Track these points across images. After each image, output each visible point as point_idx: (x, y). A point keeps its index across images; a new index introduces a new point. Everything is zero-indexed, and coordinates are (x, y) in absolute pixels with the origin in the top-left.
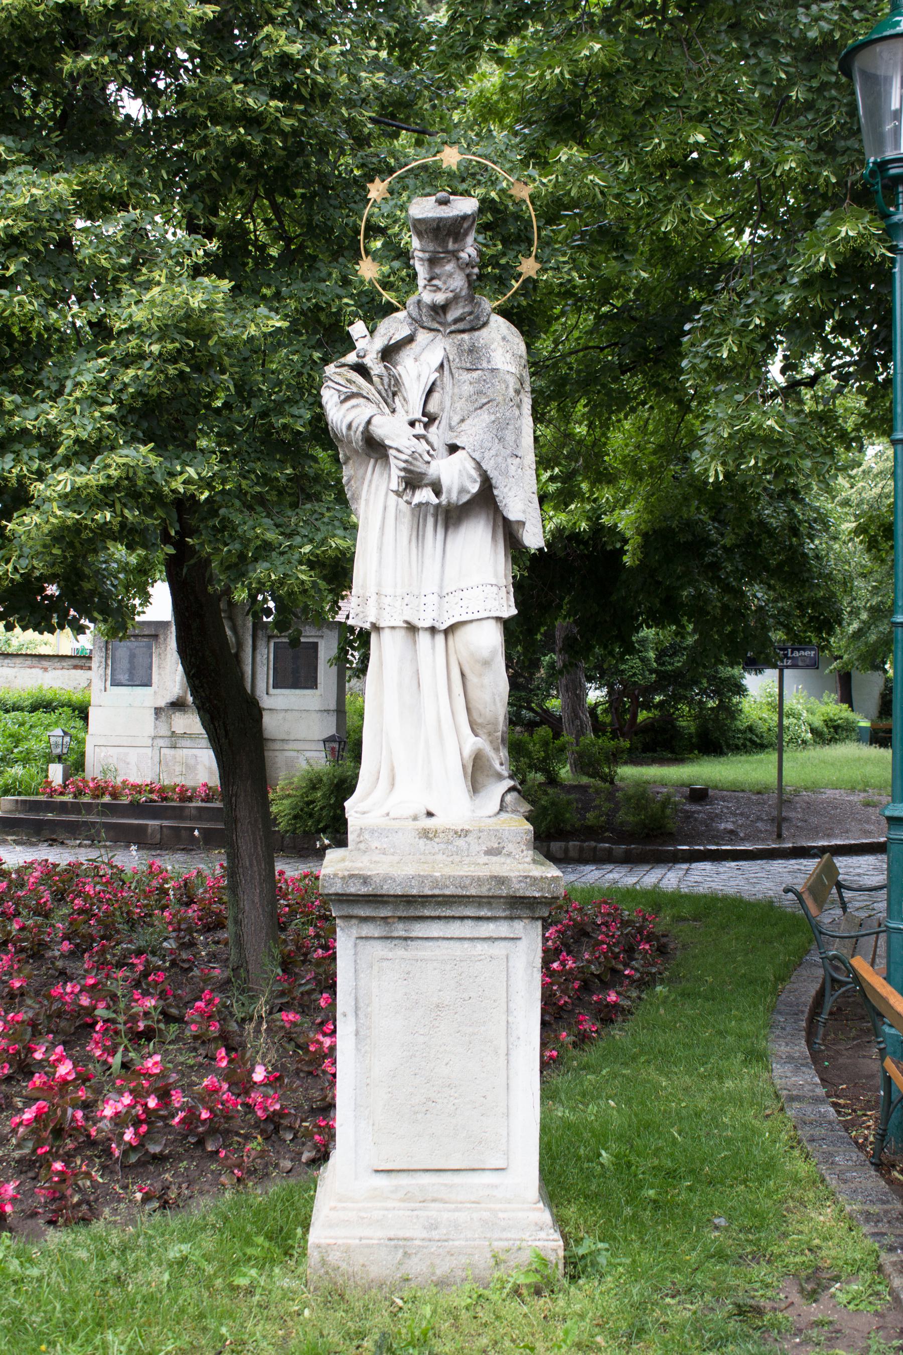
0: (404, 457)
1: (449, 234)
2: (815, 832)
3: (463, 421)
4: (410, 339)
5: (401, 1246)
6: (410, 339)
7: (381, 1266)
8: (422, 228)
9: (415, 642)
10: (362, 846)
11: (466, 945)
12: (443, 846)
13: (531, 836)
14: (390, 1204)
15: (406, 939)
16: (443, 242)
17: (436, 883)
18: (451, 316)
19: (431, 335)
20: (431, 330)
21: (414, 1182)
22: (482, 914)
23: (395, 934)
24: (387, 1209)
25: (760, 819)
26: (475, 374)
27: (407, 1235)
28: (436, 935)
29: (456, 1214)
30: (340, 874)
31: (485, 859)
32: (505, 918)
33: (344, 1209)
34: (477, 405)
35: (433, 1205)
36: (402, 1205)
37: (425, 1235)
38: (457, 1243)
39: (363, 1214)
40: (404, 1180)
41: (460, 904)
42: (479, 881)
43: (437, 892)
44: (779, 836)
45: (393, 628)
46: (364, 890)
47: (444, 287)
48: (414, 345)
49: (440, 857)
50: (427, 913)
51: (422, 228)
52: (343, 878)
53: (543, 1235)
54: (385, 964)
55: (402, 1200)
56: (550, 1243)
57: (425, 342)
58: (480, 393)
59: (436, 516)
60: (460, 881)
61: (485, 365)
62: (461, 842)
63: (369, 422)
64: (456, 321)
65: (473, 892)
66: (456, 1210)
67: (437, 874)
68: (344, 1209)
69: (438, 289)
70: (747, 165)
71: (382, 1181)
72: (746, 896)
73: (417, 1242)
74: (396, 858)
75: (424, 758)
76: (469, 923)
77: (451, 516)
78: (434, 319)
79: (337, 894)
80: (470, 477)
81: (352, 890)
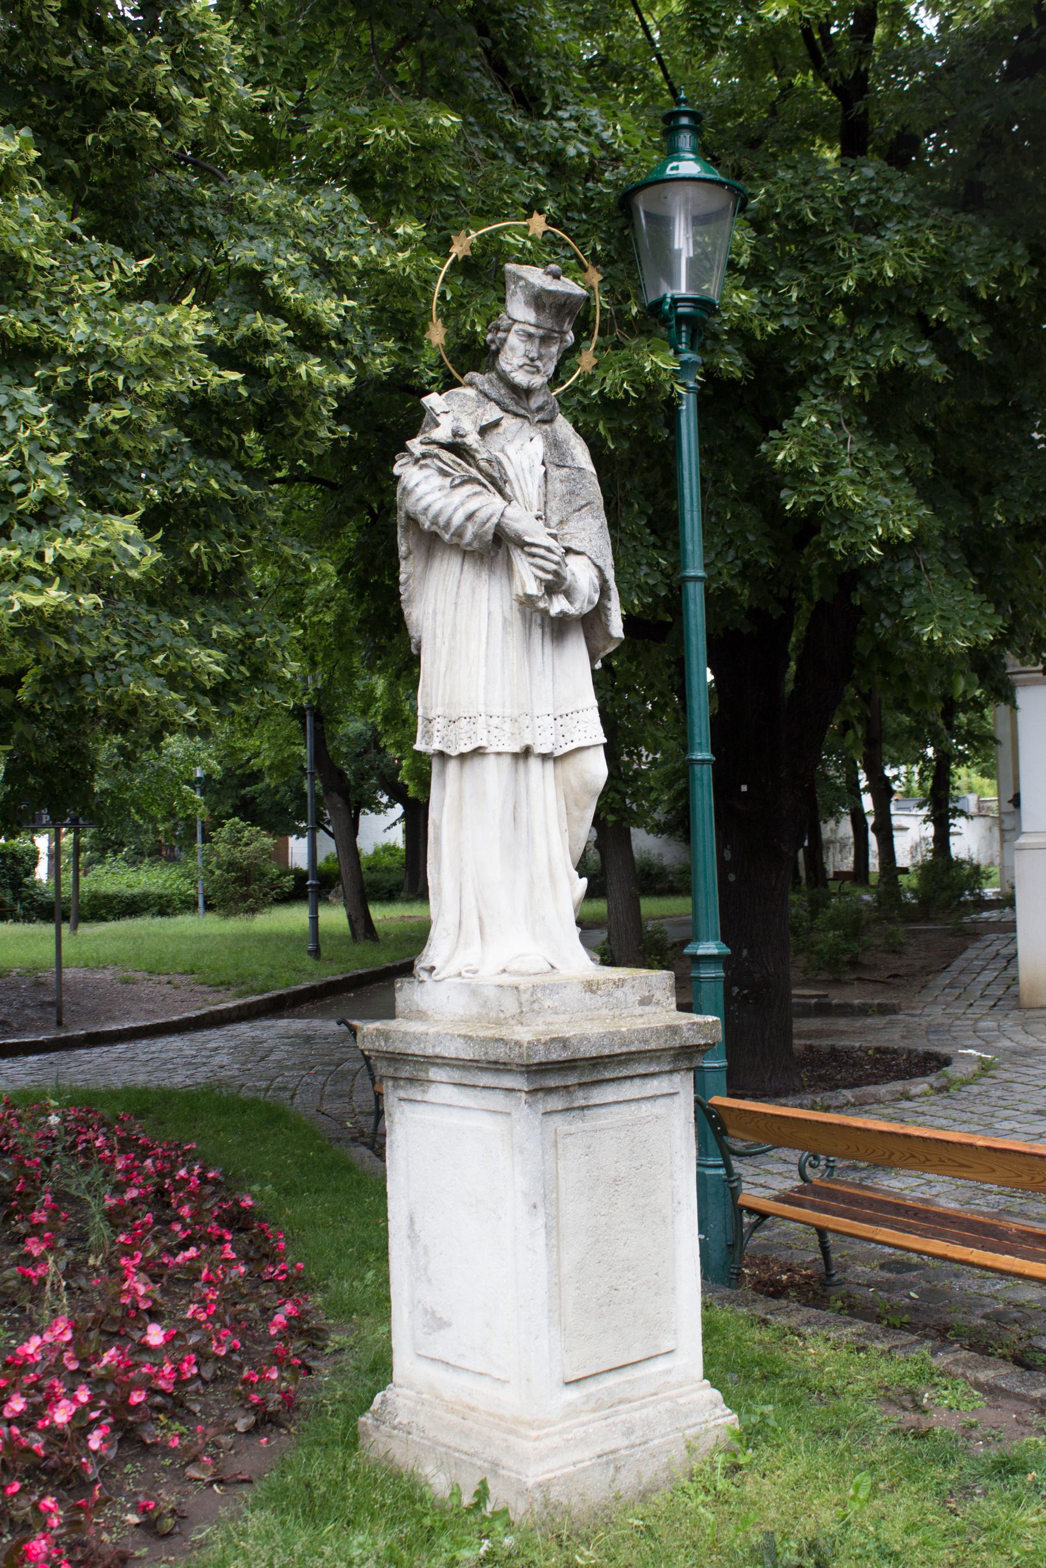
2: (94, 1015)
4: (496, 424)
5: (609, 1459)
6: (496, 424)
7: (597, 1489)
8: (547, 301)
9: (517, 770)
10: (536, 1006)
11: (634, 1107)
12: (605, 999)
13: (672, 982)
14: (585, 1418)
15: (582, 1108)
17: (624, 1040)
18: (535, 402)
19: (519, 420)
20: (516, 415)
21: (601, 1386)
22: (651, 1070)
23: (576, 1104)
24: (584, 1424)
25: (25, 1006)
27: (613, 1447)
28: (611, 1100)
29: (645, 1411)
30: (543, 1039)
31: (639, 1010)
32: (666, 1072)
33: (547, 1435)
34: (575, 506)
35: (621, 1407)
36: (597, 1415)
37: (626, 1443)
38: (656, 1442)
39: (566, 1436)
40: (591, 1388)
41: (638, 1061)
42: (656, 1032)
43: (625, 1049)
44: (59, 1023)
45: (499, 754)
46: (565, 1055)
48: (500, 430)
49: (604, 1012)
50: (608, 1075)
51: (547, 301)
52: (545, 1043)
53: (718, 1412)
54: (569, 1140)
55: (594, 1410)
56: (727, 1419)
58: (571, 493)
60: (641, 1035)
61: (570, 463)
62: (619, 993)
64: (540, 409)
65: (653, 1046)
66: (643, 1407)
67: (624, 1029)
68: (547, 1435)
69: (538, 371)
71: (573, 1394)
72: (152, 1086)
73: (623, 1452)
74: (567, 1017)
75: (505, 903)
76: (637, 1082)
77: (558, 628)
78: (517, 404)
79: (541, 1064)
81: (554, 1057)
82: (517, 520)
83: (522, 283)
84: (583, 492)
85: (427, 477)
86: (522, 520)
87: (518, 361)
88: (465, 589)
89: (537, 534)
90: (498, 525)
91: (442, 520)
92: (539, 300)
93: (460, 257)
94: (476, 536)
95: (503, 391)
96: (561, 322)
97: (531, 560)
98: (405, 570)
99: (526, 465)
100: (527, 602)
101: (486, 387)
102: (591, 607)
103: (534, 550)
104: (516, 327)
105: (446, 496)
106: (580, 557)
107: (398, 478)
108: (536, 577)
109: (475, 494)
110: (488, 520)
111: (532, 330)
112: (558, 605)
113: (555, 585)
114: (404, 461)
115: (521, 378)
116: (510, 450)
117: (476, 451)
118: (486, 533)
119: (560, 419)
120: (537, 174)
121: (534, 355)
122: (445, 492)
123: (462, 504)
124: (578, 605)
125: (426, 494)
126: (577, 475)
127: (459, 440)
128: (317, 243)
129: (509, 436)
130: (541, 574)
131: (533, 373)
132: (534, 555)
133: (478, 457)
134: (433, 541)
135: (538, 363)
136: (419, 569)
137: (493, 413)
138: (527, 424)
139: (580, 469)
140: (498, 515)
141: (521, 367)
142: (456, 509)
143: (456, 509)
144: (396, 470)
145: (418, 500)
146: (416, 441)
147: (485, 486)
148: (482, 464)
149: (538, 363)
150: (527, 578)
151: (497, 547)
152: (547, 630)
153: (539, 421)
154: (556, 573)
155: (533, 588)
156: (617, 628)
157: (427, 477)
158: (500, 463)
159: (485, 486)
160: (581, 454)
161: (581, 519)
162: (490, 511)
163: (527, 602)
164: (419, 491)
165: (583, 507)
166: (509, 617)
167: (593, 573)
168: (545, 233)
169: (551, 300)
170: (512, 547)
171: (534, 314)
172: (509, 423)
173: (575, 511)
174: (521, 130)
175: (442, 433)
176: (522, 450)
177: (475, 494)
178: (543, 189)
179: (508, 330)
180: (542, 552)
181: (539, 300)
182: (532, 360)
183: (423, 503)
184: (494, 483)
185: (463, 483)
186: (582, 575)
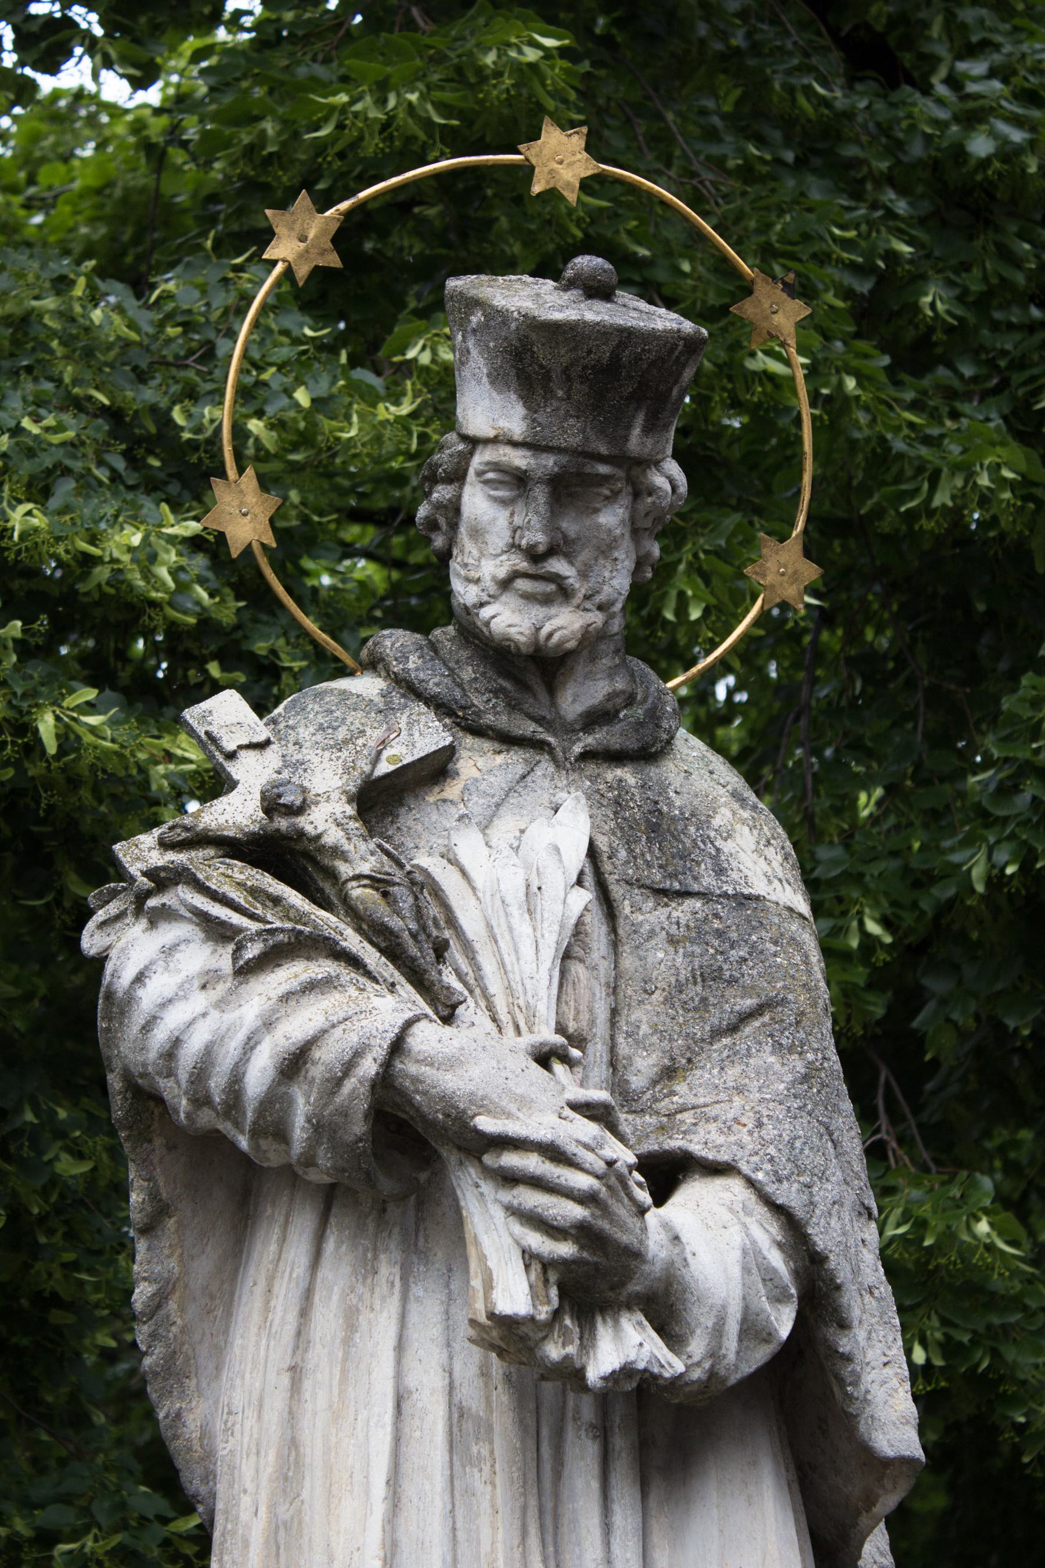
0: (582, 1181)
1: (636, 398)
3: (669, 1073)
4: (436, 769)
6: (436, 769)
16: (615, 426)
18: (578, 697)
19: (514, 761)
20: (508, 740)
26: (685, 911)
34: (715, 1018)
47: (581, 589)
48: (452, 790)
51: (552, 358)
57: (498, 782)
58: (709, 976)
59: (603, 1434)
61: (708, 881)
63: (398, 1047)
64: (597, 718)
69: (564, 593)
70: (294, 496)
77: (661, 1436)
78: (513, 706)
80: (769, 1276)
82: (452, 1063)
83: (476, 318)
84: (751, 972)
85: (169, 951)
86: (478, 1066)
87: (493, 568)
88: (326, 1319)
89: (536, 1108)
90: (385, 1082)
91: (217, 1083)
92: (530, 360)
93: (302, 272)
94: (319, 1127)
95: (467, 673)
96: (615, 426)
97: (507, 1196)
98: (149, 1267)
99: (513, 886)
100: (508, 1337)
101: (413, 662)
102: (761, 1355)
103: (511, 1160)
104: (480, 458)
105: (221, 1004)
106: (719, 1183)
107: (100, 961)
108: (529, 1257)
109: (311, 987)
110: (349, 1067)
111: (520, 459)
112: (622, 1345)
113: (596, 1277)
114: (113, 908)
115: (509, 619)
116: (469, 845)
117: (337, 852)
118: (344, 1113)
119: (689, 747)
120: (890, 214)
121: (537, 537)
122: (221, 988)
123: (268, 1024)
124: (697, 1346)
125: (166, 1004)
126: (729, 917)
127: (282, 823)
128: (149, 394)
129: (477, 805)
130: (536, 1241)
131: (546, 600)
132: (510, 1179)
133: (345, 870)
134: (232, 1167)
135: (558, 566)
136: (204, 1267)
137: (422, 735)
138: (546, 766)
139: (744, 900)
140: (379, 1050)
141: (505, 584)
142: (250, 1045)
143: (250, 1045)
144: (91, 941)
145: (147, 1027)
146: (148, 840)
147: (354, 962)
148: (357, 892)
149: (558, 566)
150: (504, 1267)
151: (401, 1160)
152: (619, 1442)
153: (586, 756)
154: (582, 1233)
155: (514, 1295)
156: (892, 1418)
157: (169, 951)
158: (437, 893)
159: (354, 962)
160: (755, 856)
161: (734, 1056)
162: (354, 1039)
163: (508, 1339)
164: (148, 997)
165: (746, 1017)
166: (471, 1394)
167: (765, 1234)
168: (586, 185)
169: (564, 355)
170: (451, 1157)
171: (519, 410)
172: (480, 766)
173: (717, 1034)
174: (849, 115)
175: (236, 812)
176: (514, 853)
177: (311, 987)
178: (906, 249)
179: (457, 477)
180: (532, 1163)
181: (530, 360)
182: (534, 556)
183: (160, 1036)
184: (393, 952)
185: (274, 956)
186: (713, 1241)
